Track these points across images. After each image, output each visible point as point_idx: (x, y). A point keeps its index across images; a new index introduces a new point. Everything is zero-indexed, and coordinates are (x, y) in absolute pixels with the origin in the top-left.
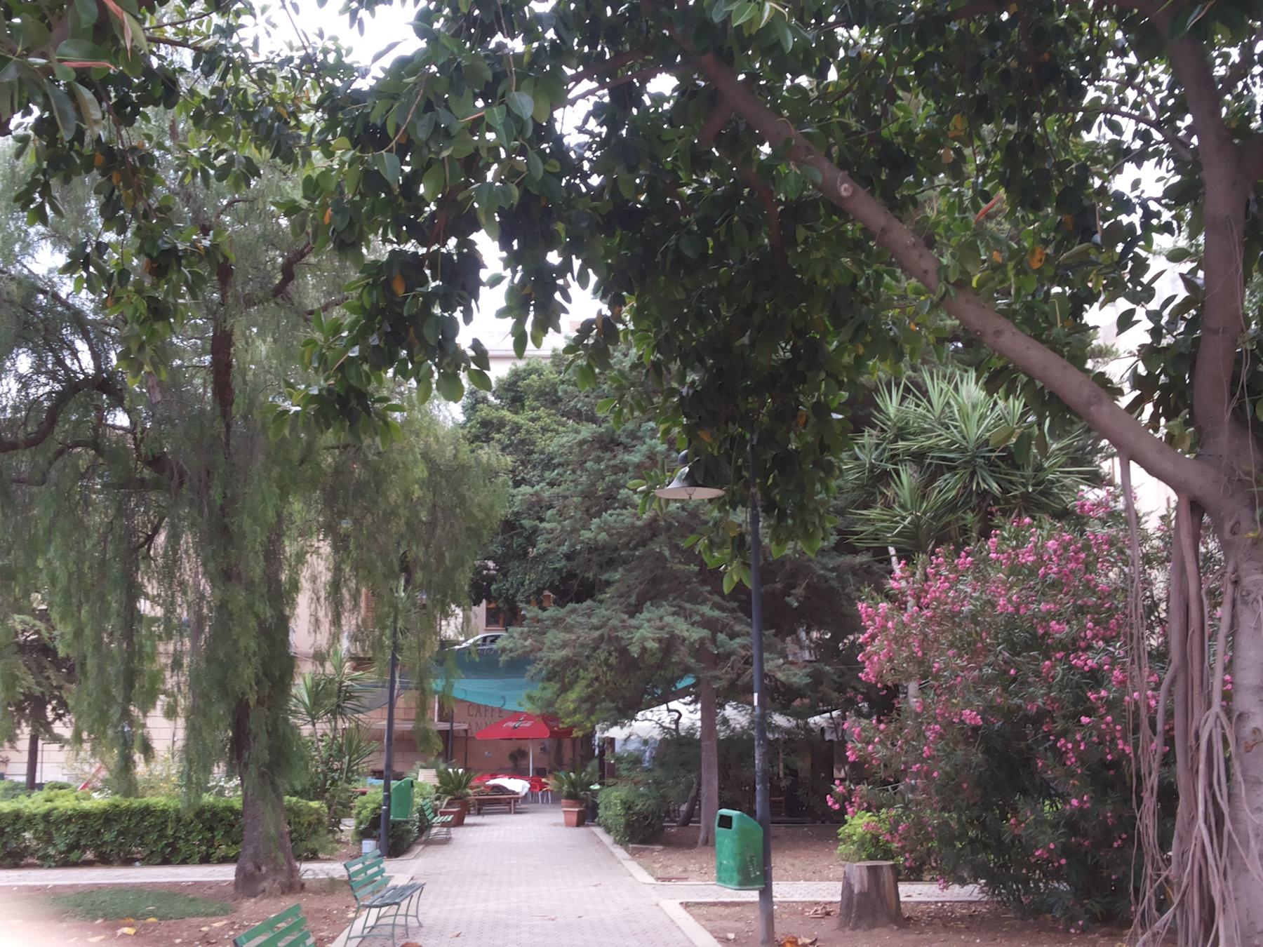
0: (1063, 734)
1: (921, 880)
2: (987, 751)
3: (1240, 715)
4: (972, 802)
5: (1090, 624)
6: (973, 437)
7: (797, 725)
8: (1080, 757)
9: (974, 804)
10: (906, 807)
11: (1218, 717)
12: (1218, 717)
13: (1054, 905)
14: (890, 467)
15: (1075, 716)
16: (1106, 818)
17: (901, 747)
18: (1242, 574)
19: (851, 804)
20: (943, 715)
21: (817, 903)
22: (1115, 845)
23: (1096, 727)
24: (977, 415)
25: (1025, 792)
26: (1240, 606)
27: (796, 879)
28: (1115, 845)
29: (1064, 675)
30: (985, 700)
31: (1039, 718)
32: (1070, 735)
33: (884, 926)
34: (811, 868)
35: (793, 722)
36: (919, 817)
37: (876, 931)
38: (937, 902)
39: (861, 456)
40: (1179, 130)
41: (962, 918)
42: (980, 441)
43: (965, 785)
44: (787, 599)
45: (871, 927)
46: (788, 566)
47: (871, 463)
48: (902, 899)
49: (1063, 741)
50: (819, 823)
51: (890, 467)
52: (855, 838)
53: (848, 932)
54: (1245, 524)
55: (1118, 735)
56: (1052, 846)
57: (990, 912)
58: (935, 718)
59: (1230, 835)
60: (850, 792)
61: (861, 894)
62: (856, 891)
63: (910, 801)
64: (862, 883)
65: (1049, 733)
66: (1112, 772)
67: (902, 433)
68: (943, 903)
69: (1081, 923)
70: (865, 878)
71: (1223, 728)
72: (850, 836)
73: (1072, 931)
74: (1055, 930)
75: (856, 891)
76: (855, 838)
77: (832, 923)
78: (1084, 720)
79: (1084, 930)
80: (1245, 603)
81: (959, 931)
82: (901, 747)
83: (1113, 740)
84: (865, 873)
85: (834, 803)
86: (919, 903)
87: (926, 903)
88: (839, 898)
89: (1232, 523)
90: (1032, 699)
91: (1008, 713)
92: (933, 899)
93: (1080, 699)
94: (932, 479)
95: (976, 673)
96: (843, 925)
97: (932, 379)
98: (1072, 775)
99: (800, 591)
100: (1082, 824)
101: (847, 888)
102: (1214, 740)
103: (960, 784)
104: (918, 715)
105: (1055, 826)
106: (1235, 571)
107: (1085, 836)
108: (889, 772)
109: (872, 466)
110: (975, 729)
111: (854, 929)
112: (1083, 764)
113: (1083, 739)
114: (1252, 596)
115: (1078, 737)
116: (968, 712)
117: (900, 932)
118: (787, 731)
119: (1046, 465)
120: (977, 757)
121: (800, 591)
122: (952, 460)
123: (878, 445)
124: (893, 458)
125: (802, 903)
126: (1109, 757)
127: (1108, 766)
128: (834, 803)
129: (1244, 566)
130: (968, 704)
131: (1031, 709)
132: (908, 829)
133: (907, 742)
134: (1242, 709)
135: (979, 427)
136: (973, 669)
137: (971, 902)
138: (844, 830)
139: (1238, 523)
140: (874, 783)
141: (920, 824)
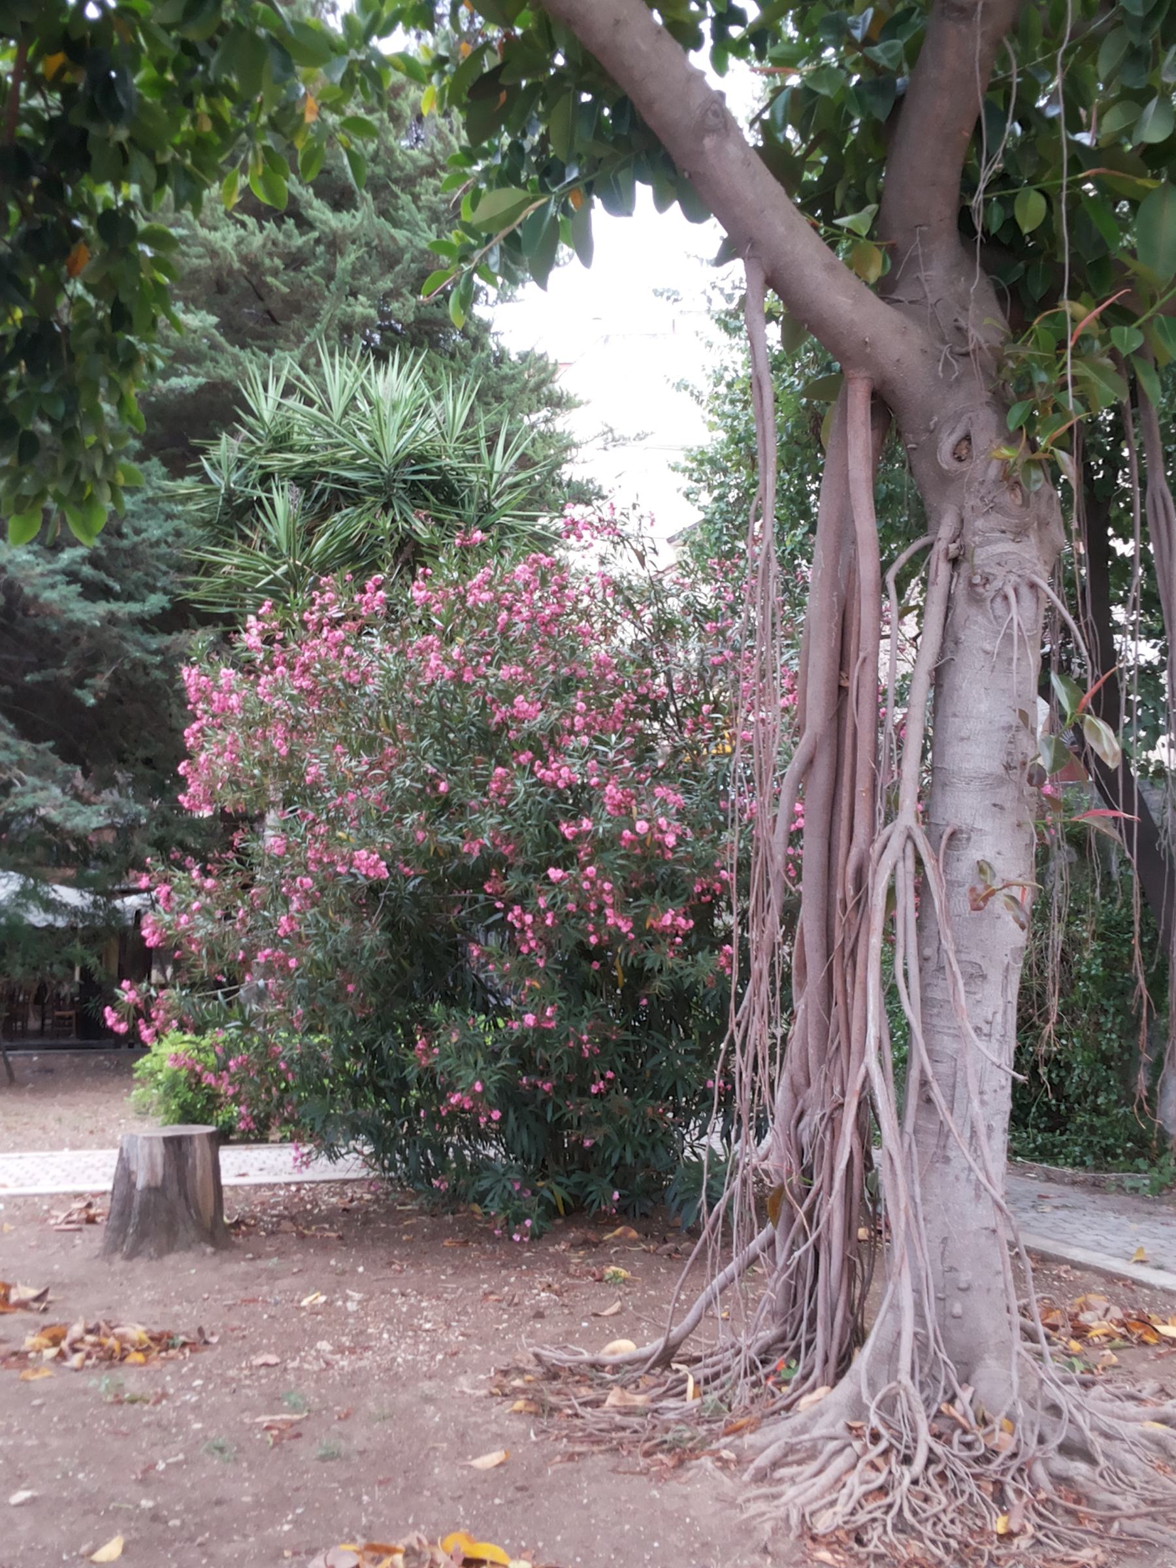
0: (522, 898)
1: (265, 1141)
2: (390, 927)
3: (953, 835)
4: (359, 1016)
5: (581, 706)
6: (391, 451)
7: (95, 902)
8: (547, 942)
9: (364, 1021)
10: (246, 1027)
11: (909, 837)
12: (909, 837)
13: (486, 1192)
14: (259, 493)
15: (538, 870)
16: (580, 1043)
17: (243, 921)
18: (972, 540)
19: (149, 1020)
20: (319, 862)
21: (78, 1196)
22: (594, 1090)
23: (574, 887)
24: (397, 419)
25: (449, 1000)
26: (962, 607)
27: (56, 1146)
28: (594, 1090)
29: (528, 795)
30: (397, 835)
31: (492, 863)
32: (529, 902)
33: (188, 1247)
34: (89, 1124)
35: (89, 898)
36: (266, 1045)
37: (171, 1260)
38: (288, 1184)
39: (213, 476)
40: (239, 1113)
41: (329, 1217)
42: (402, 455)
43: (350, 988)
44: (79, 693)
45: (161, 1253)
46: (84, 642)
47: (228, 488)
48: (227, 1179)
49: (517, 910)
50: (124, 1048)
51: (259, 493)
52: (160, 1076)
53: (119, 1262)
54: (981, 439)
55: (609, 900)
56: (478, 1087)
57: (377, 1201)
58: (306, 867)
59: (924, 1083)
60: (149, 1001)
61: (150, 1189)
62: (141, 1182)
63: (254, 1016)
64: (152, 1169)
65: (498, 895)
66: (596, 965)
67: (281, 443)
68: (299, 1185)
69: (528, 1223)
70: (159, 1161)
71: (919, 862)
72: (152, 1074)
73: (516, 1237)
74: (487, 1233)
75: (141, 1182)
76: (160, 1076)
77: (96, 1237)
78: (554, 873)
79: (536, 1236)
80: (975, 598)
81: (325, 1246)
82: (243, 921)
83: (600, 910)
84: (159, 1150)
85: (119, 1021)
86: (258, 1187)
87: (271, 1186)
88: (109, 1186)
89: (954, 438)
90: (475, 834)
91: (438, 857)
92: (283, 1179)
93: (551, 838)
94: (324, 515)
95: (384, 785)
96: (111, 1248)
97: (333, 366)
98: (529, 969)
99: (101, 681)
100: (540, 1053)
101: (125, 1175)
102: (900, 885)
103: (341, 987)
104: (277, 861)
105: (495, 1056)
106: (958, 536)
107: (544, 1074)
108: (217, 965)
109: (230, 493)
110: (375, 889)
111: (129, 1257)
112: (550, 950)
113: (549, 908)
114: (997, 584)
115: (542, 902)
116: (363, 853)
117: (216, 1260)
118: (75, 912)
119: (496, 504)
120: (373, 936)
121: (101, 681)
122: (354, 484)
123: (241, 462)
124: (266, 478)
125: (52, 1196)
126: (593, 940)
127: (584, 952)
128: (119, 1021)
129: (980, 524)
130: (366, 841)
131: (472, 850)
132: (245, 1066)
133: (253, 911)
134: (955, 823)
135: (400, 436)
136: (377, 780)
137: (345, 1182)
138: (145, 1063)
139: (967, 438)
140: (192, 986)
141: (266, 1052)
